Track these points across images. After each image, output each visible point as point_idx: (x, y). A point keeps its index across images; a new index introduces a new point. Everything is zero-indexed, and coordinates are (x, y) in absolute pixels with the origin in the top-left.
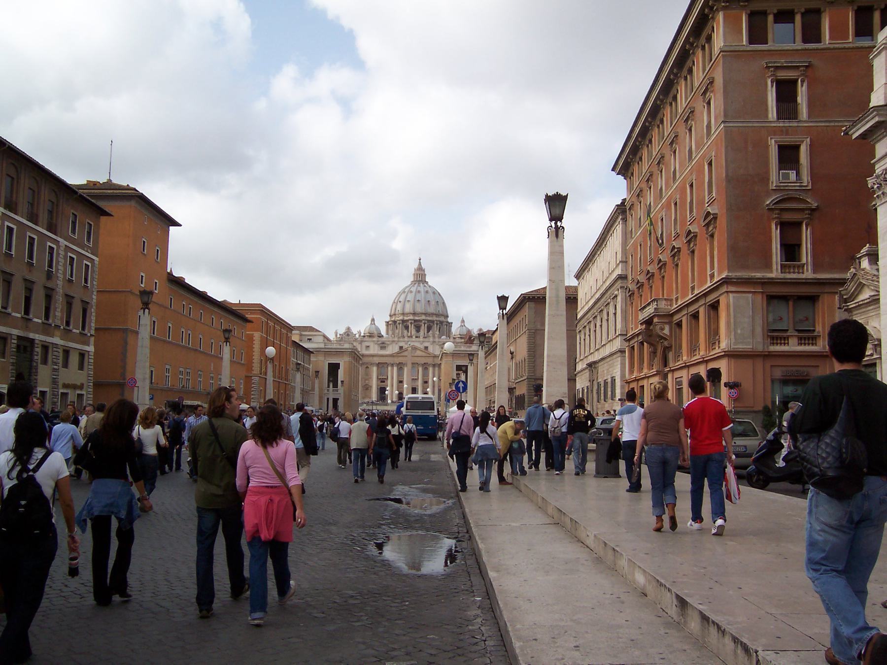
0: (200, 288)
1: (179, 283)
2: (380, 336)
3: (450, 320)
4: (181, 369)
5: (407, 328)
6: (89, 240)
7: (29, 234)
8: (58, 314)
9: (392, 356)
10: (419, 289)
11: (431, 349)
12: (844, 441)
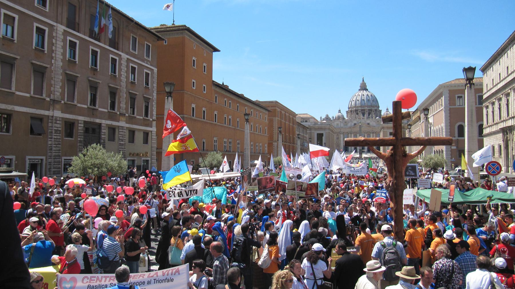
0: (239, 92)
1: (224, 88)
2: (344, 119)
3: (380, 109)
4: (225, 140)
5: (358, 114)
6: (148, 56)
7: (91, 47)
8: (123, 105)
9: (350, 127)
10: (363, 93)
11: (371, 124)
12: (313, 147)
